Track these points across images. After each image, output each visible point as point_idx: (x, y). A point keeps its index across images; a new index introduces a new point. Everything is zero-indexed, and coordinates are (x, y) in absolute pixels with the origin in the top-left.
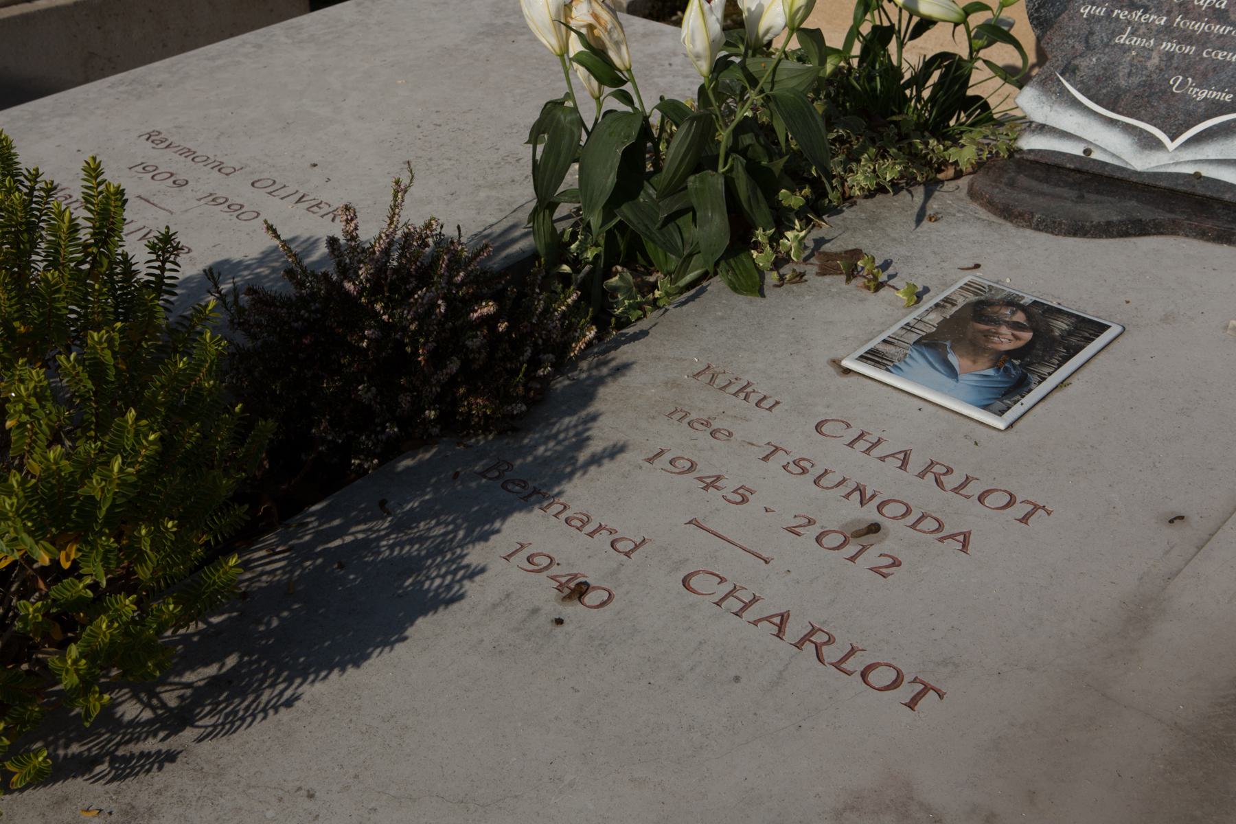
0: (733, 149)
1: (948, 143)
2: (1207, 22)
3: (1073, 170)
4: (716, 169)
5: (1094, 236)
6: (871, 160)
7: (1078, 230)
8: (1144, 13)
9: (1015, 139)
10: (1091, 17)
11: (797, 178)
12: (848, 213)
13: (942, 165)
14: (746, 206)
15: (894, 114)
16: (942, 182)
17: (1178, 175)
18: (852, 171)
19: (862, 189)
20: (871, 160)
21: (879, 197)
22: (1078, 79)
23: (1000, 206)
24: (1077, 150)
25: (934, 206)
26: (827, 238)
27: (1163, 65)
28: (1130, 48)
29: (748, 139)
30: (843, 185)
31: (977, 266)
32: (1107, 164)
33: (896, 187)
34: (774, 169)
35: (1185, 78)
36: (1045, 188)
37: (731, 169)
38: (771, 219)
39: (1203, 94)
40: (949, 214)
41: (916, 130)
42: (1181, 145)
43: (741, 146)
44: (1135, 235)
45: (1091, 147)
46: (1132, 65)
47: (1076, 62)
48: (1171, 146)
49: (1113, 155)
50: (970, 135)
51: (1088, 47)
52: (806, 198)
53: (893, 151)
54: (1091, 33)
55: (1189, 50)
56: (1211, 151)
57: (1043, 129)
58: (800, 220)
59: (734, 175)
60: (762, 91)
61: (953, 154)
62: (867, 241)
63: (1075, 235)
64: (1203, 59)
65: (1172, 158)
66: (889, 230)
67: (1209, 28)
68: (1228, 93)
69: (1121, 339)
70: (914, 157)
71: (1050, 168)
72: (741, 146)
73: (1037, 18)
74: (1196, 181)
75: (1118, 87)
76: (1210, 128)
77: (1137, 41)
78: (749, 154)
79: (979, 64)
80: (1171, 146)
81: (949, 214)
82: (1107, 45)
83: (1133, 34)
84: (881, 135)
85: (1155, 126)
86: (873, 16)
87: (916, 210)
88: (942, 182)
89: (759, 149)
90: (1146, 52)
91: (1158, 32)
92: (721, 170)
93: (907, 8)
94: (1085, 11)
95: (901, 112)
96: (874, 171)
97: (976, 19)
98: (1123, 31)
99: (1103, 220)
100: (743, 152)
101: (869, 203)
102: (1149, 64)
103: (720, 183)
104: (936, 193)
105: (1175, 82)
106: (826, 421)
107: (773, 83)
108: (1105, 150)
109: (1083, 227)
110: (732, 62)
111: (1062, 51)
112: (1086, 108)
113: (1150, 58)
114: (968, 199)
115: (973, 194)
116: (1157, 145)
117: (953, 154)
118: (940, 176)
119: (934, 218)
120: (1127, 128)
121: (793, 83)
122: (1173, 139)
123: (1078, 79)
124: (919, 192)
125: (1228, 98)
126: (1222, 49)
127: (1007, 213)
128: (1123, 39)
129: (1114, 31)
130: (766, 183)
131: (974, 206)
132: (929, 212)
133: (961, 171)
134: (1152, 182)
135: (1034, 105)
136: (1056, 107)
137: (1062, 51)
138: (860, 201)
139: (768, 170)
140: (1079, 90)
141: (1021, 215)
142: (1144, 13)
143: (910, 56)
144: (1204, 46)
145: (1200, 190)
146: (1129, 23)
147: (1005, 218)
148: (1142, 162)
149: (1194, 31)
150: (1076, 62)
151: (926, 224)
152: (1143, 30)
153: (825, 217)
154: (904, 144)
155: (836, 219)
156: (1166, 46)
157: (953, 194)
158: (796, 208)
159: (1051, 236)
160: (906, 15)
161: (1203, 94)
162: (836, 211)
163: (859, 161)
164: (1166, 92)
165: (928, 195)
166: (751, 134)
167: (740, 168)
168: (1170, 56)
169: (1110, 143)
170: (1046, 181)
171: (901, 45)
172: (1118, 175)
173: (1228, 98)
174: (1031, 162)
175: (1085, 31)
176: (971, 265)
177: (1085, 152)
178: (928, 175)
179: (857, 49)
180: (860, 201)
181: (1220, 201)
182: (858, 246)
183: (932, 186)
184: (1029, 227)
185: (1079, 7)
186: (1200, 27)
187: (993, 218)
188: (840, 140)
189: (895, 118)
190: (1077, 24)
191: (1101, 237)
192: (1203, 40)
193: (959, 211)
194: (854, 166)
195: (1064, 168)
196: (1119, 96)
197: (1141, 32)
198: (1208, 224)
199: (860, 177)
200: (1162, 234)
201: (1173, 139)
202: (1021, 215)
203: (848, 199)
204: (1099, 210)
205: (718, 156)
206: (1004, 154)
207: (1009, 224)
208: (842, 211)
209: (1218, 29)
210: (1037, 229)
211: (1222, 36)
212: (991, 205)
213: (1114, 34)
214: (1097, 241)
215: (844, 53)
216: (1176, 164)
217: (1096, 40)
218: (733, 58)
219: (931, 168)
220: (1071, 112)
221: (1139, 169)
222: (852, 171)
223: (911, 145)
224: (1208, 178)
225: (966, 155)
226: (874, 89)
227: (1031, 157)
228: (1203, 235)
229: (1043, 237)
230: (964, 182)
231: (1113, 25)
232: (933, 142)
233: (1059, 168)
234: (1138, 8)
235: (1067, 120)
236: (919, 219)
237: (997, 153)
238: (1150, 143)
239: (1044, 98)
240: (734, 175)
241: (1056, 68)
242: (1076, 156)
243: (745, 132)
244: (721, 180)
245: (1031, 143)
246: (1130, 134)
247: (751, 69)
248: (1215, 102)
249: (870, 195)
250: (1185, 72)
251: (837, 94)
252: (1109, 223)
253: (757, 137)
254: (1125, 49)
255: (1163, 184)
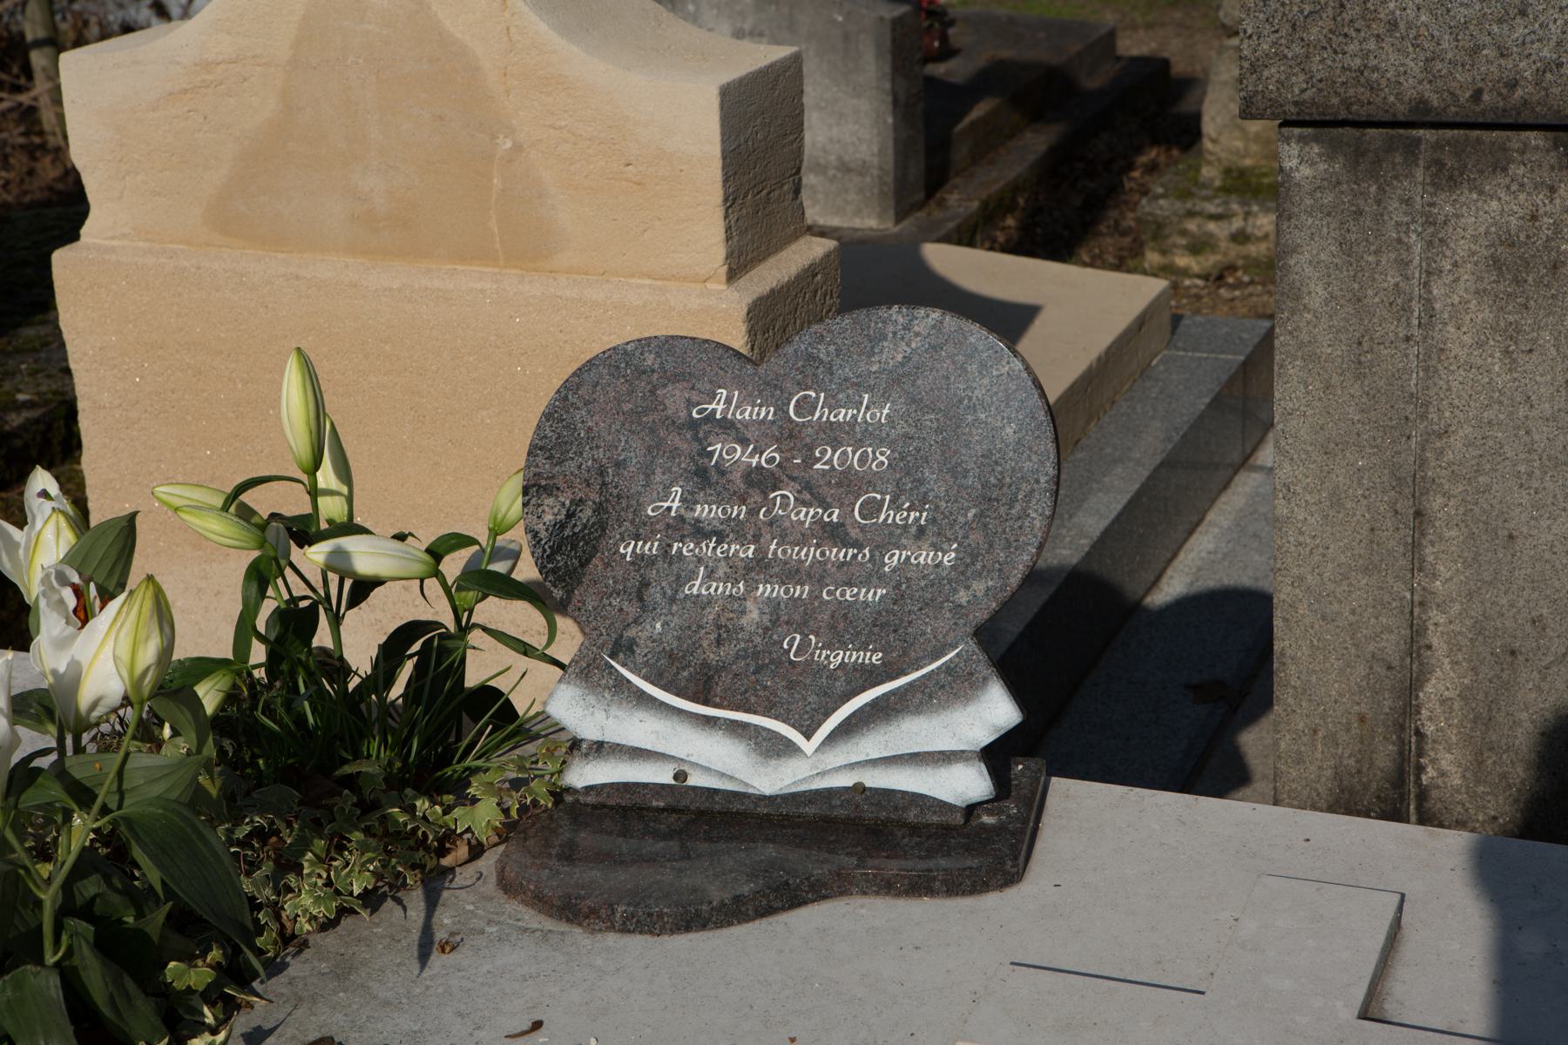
0: (67, 909)
1: (449, 798)
2: (818, 546)
3: (664, 810)
4: (40, 961)
5: (720, 925)
6: (320, 860)
7: (692, 920)
8: (719, 543)
9: (560, 772)
10: (639, 559)
11: (190, 929)
12: (297, 967)
13: (447, 839)
14: (106, 1011)
15: (344, 762)
16: (452, 870)
17: (830, 793)
18: (289, 890)
19: (313, 918)
20: (320, 860)
21: (346, 922)
22: (639, 660)
23: (557, 903)
24: (661, 775)
25: (445, 920)
26: (267, 1026)
27: (766, 618)
28: (710, 601)
29: (90, 887)
30: (278, 917)
31: (537, 1025)
32: (716, 791)
33: (371, 899)
34: (147, 930)
35: (805, 636)
36: (624, 845)
37: (70, 952)
38: (158, 1022)
39: (837, 659)
40: (473, 931)
41: (390, 787)
42: (823, 743)
43: (79, 901)
44: (783, 909)
45: (686, 768)
46: (719, 627)
47: (631, 632)
48: (808, 746)
49: (723, 775)
50: (487, 777)
51: (644, 608)
52: (217, 967)
53: (357, 836)
54: (645, 584)
55: (801, 591)
56: (872, 745)
57: (600, 749)
58: (212, 1005)
59: (76, 961)
60: (105, 810)
61: (461, 818)
62: (339, 1017)
63: (688, 929)
64: (823, 603)
65: (813, 765)
66: (374, 985)
67: (823, 554)
68: (874, 651)
69: (855, 935)
70: (391, 840)
71: (627, 810)
72: (79, 901)
73: (554, 571)
74: (858, 798)
75: (705, 664)
76: (861, 710)
77: (719, 588)
78: (98, 908)
79: (475, 637)
80: (808, 746)
81: (473, 931)
82: (673, 600)
83: (710, 575)
84: (330, 809)
85: (776, 718)
86: (277, 588)
87: (416, 935)
88: (452, 870)
89: (115, 899)
90: (736, 604)
91: (748, 569)
92: (51, 959)
93: (334, 571)
94: (627, 550)
95: (357, 756)
96: (329, 883)
97: (453, 566)
98: (692, 575)
99: (727, 896)
100: (86, 912)
101: (330, 939)
102: (744, 621)
103: (52, 984)
104: (445, 894)
105: (791, 645)
106: (405, 909)
107: (121, 793)
108: (707, 770)
109: (698, 914)
110: (39, 770)
111: (604, 618)
112: (663, 704)
113: (743, 612)
114: (501, 896)
115: (507, 886)
116: (786, 749)
117: (461, 818)
118: (446, 861)
119: (448, 947)
120: (736, 728)
121: (157, 789)
122: (808, 737)
123: (639, 660)
124: (415, 900)
125: (876, 658)
126: (850, 584)
127: (570, 910)
128: (696, 587)
129: (678, 577)
130: (132, 956)
131: (513, 907)
132: (440, 935)
133: (480, 844)
134: (793, 810)
135: (579, 711)
136: (614, 710)
137: (604, 618)
138: (317, 939)
139: (139, 935)
140: (646, 678)
141: (593, 912)
142: (719, 543)
143: (359, 640)
144: (821, 582)
145: (868, 812)
146: (700, 560)
147: (568, 920)
148: (771, 780)
149: (800, 561)
150: (631, 632)
151: (437, 960)
152: (722, 570)
153: (255, 984)
154: (373, 820)
155: (277, 984)
156: (765, 590)
157: (473, 891)
158: (201, 989)
159: (648, 937)
160: (333, 578)
161: (837, 659)
162: (275, 968)
163: (298, 869)
164: (781, 662)
165: (432, 902)
166: (95, 878)
167: (86, 951)
168: (774, 605)
169: (709, 754)
170: (625, 833)
171: (336, 620)
172: (736, 806)
173: (876, 658)
174: (594, 807)
175: (634, 582)
176: (527, 1025)
177: (676, 777)
178: (424, 862)
179: (258, 653)
180: (317, 939)
181: (902, 824)
182: (325, 1032)
183: (435, 882)
184: (612, 928)
185: (617, 545)
186: (808, 554)
187: (549, 924)
188: (258, 833)
189: (348, 769)
190: (620, 573)
191: (730, 924)
192: (818, 575)
193: (489, 922)
194: (292, 879)
195: (648, 809)
196: (710, 678)
197: (720, 573)
198: (893, 867)
199: (306, 900)
200: (825, 897)
201: (808, 737)
202: (593, 912)
203: (287, 938)
204: (720, 872)
205: (39, 928)
206: (547, 802)
207: (578, 930)
208: (284, 966)
209: (836, 554)
210: (625, 930)
211: (844, 564)
212: (540, 902)
213: (680, 581)
214: (725, 932)
215: (236, 664)
216: (823, 774)
217: (654, 594)
218: (37, 763)
219: (427, 849)
220: (640, 714)
221: (767, 792)
222: (289, 890)
223: (385, 819)
224: (876, 790)
225: (483, 816)
226: (301, 720)
227: (590, 799)
228: (888, 887)
229: (637, 942)
230: (488, 862)
231: (674, 567)
232: (422, 805)
233: (640, 811)
234: (708, 536)
235: (636, 728)
236: (424, 957)
237: (535, 803)
238: (779, 748)
239: (591, 699)
240: (76, 961)
241: (601, 647)
242: (663, 786)
243: (84, 876)
244: (54, 981)
245: (585, 775)
246: (740, 736)
247: (78, 774)
248: (860, 668)
249: (327, 925)
250: (802, 627)
251: (238, 750)
252: (737, 899)
253: (107, 879)
254: (701, 603)
255: (810, 810)
